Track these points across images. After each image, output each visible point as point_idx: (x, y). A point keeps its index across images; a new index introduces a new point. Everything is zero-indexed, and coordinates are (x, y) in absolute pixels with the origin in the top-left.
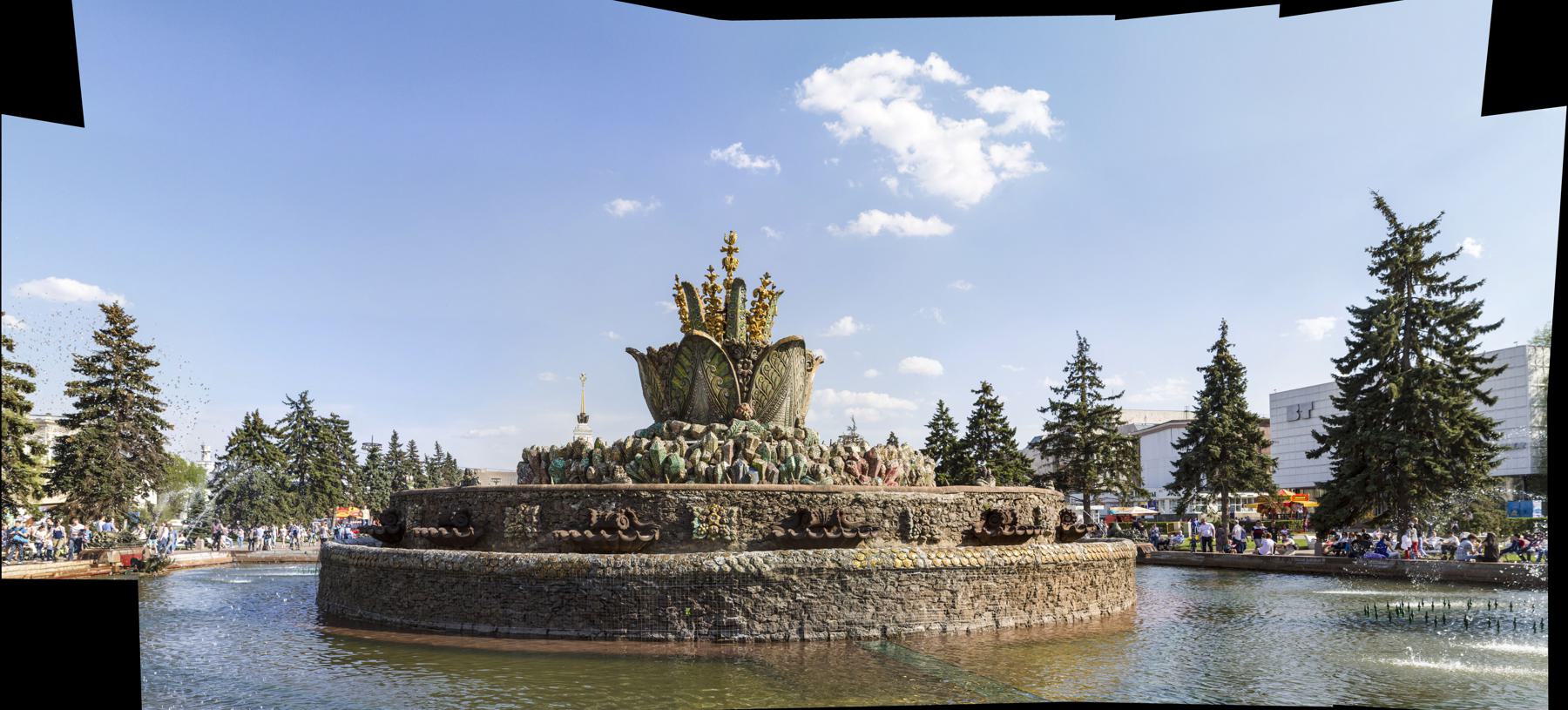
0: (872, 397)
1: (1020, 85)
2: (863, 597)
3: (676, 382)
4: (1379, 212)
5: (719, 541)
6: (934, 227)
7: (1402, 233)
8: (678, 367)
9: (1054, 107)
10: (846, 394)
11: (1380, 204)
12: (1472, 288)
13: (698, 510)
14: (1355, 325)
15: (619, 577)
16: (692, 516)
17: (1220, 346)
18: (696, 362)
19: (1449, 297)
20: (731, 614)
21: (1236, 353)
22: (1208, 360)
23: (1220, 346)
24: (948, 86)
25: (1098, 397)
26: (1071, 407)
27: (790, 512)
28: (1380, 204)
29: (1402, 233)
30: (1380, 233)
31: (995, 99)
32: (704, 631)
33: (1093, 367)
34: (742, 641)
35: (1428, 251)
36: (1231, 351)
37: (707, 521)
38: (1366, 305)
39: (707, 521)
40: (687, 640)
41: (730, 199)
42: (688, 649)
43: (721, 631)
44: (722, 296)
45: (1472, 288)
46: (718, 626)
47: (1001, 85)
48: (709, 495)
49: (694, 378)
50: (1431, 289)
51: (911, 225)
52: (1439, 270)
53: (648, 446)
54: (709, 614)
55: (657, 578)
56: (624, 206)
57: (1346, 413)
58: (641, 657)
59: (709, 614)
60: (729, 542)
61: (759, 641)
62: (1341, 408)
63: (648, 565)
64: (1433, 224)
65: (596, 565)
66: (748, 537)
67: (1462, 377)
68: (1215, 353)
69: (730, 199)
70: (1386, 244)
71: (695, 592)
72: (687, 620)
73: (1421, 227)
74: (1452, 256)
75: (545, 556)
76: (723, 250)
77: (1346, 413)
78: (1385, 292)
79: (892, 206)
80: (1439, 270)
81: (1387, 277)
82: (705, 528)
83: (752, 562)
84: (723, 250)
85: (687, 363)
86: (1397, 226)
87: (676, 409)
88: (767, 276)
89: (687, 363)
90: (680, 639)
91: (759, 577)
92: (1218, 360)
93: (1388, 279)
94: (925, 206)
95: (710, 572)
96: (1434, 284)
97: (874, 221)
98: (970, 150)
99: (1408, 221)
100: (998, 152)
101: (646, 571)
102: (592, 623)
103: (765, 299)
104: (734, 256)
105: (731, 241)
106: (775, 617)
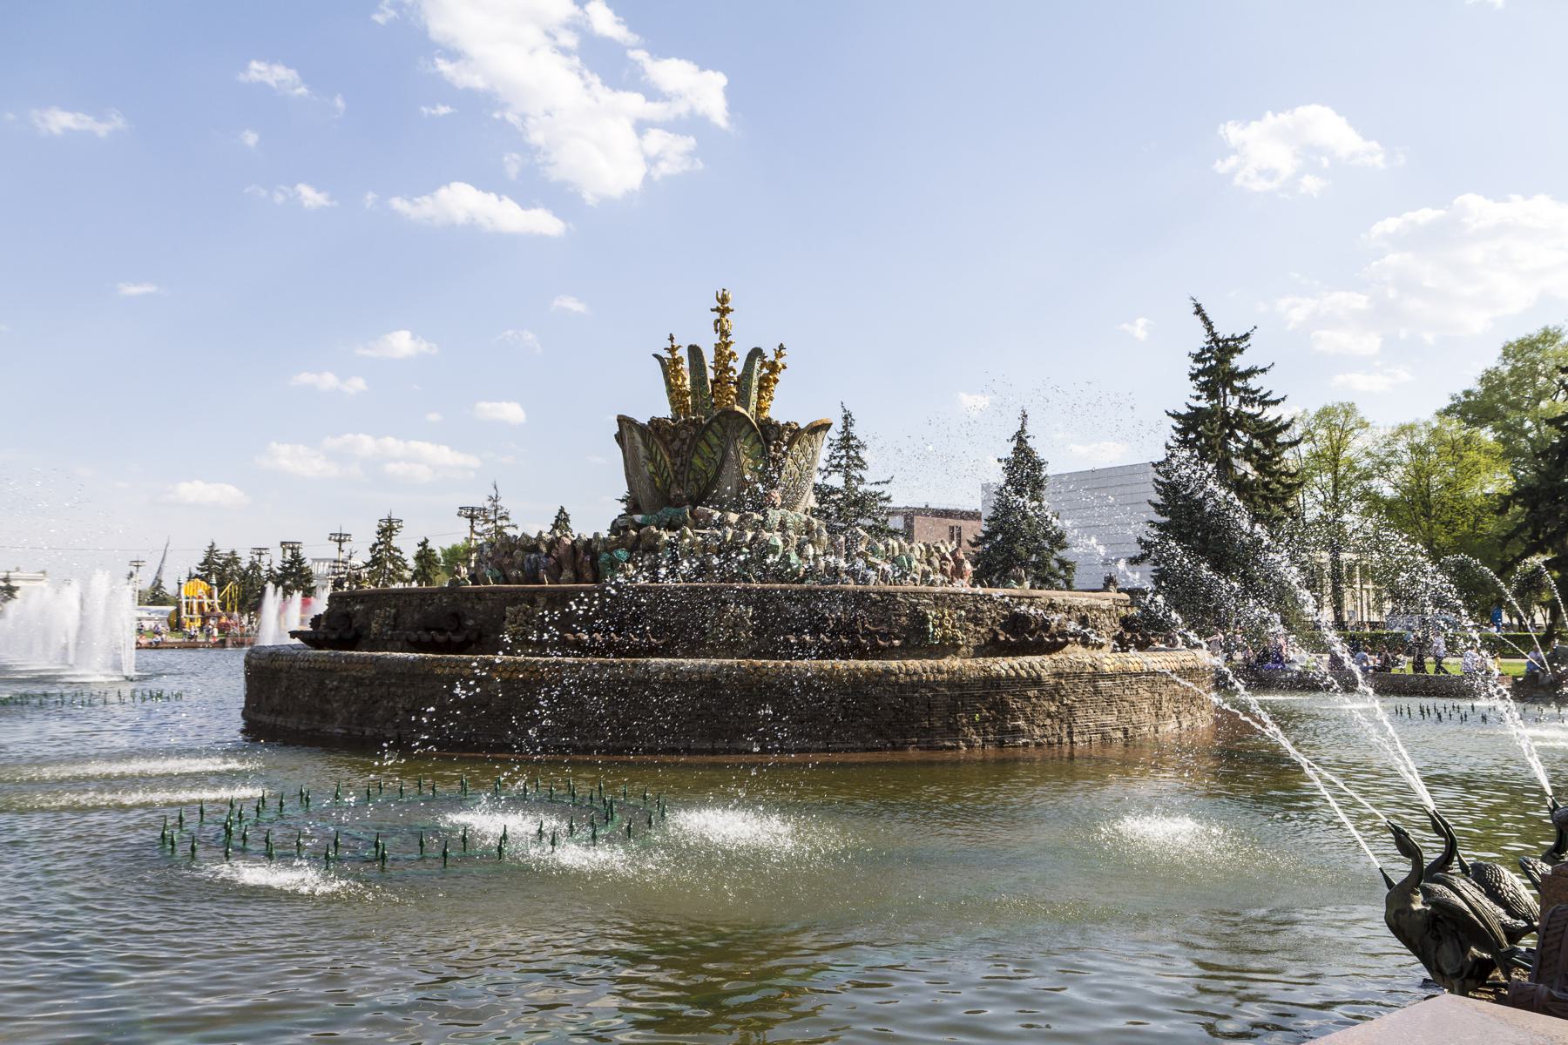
0: (427, 449)
1: (704, 64)
2: (1110, 700)
3: (697, 461)
4: (1198, 317)
5: (949, 647)
6: (543, 222)
7: (1217, 342)
8: (702, 445)
9: (732, 94)
10: (390, 441)
11: (1199, 310)
12: (1276, 402)
13: (931, 614)
14: (1178, 431)
15: (913, 684)
16: (925, 620)
17: (1020, 438)
18: (726, 441)
19: (1256, 410)
20: (1014, 719)
21: (1037, 445)
22: (1008, 451)
23: (1020, 438)
24: (608, 42)
25: (861, 480)
26: (833, 491)
27: (1004, 617)
28: (1199, 310)
29: (1217, 342)
30: (1200, 340)
31: (674, 73)
32: (991, 737)
33: (861, 446)
34: (1026, 745)
35: (1239, 362)
36: (1030, 443)
37: (941, 625)
38: (1184, 411)
39: (941, 625)
40: (974, 745)
41: (251, 138)
42: (978, 754)
43: (1005, 735)
44: (738, 366)
45: (1276, 402)
46: (1003, 731)
47: (679, 58)
48: (936, 598)
49: (723, 460)
50: (1242, 400)
51: (508, 215)
52: (1253, 383)
53: (754, 538)
54: (995, 719)
55: (950, 684)
56: (61, 121)
57: (1167, 519)
58: (931, 763)
59: (995, 719)
60: (959, 647)
61: (1038, 745)
62: (1163, 514)
63: (940, 671)
64: (1247, 335)
65: (888, 672)
66: (974, 642)
67: (1272, 491)
68: (1014, 444)
69: (251, 138)
70: (1203, 351)
71: (983, 698)
72: (976, 726)
73: (1233, 339)
74: (1263, 371)
75: (827, 664)
76: (718, 310)
77: (1167, 519)
78: (1198, 398)
79: (490, 181)
80: (1253, 383)
81: (1204, 383)
82: (939, 632)
83: (1031, 666)
84: (718, 310)
85: (715, 441)
86: (1214, 335)
87: (695, 492)
88: (781, 347)
89: (715, 441)
90: (970, 746)
91: (1037, 682)
92: (1017, 450)
93: (1203, 387)
94: (534, 187)
95: (999, 676)
96: (1249, 397)
97: (463, 201)
98: (620, 133)
99: (1223, 332)
100: (656, 140)
101: (939, 677)
102: (880, 735)
103: (765, 369)
104: (728, 316)
105: (724, 300)
106: (1048, 722)
